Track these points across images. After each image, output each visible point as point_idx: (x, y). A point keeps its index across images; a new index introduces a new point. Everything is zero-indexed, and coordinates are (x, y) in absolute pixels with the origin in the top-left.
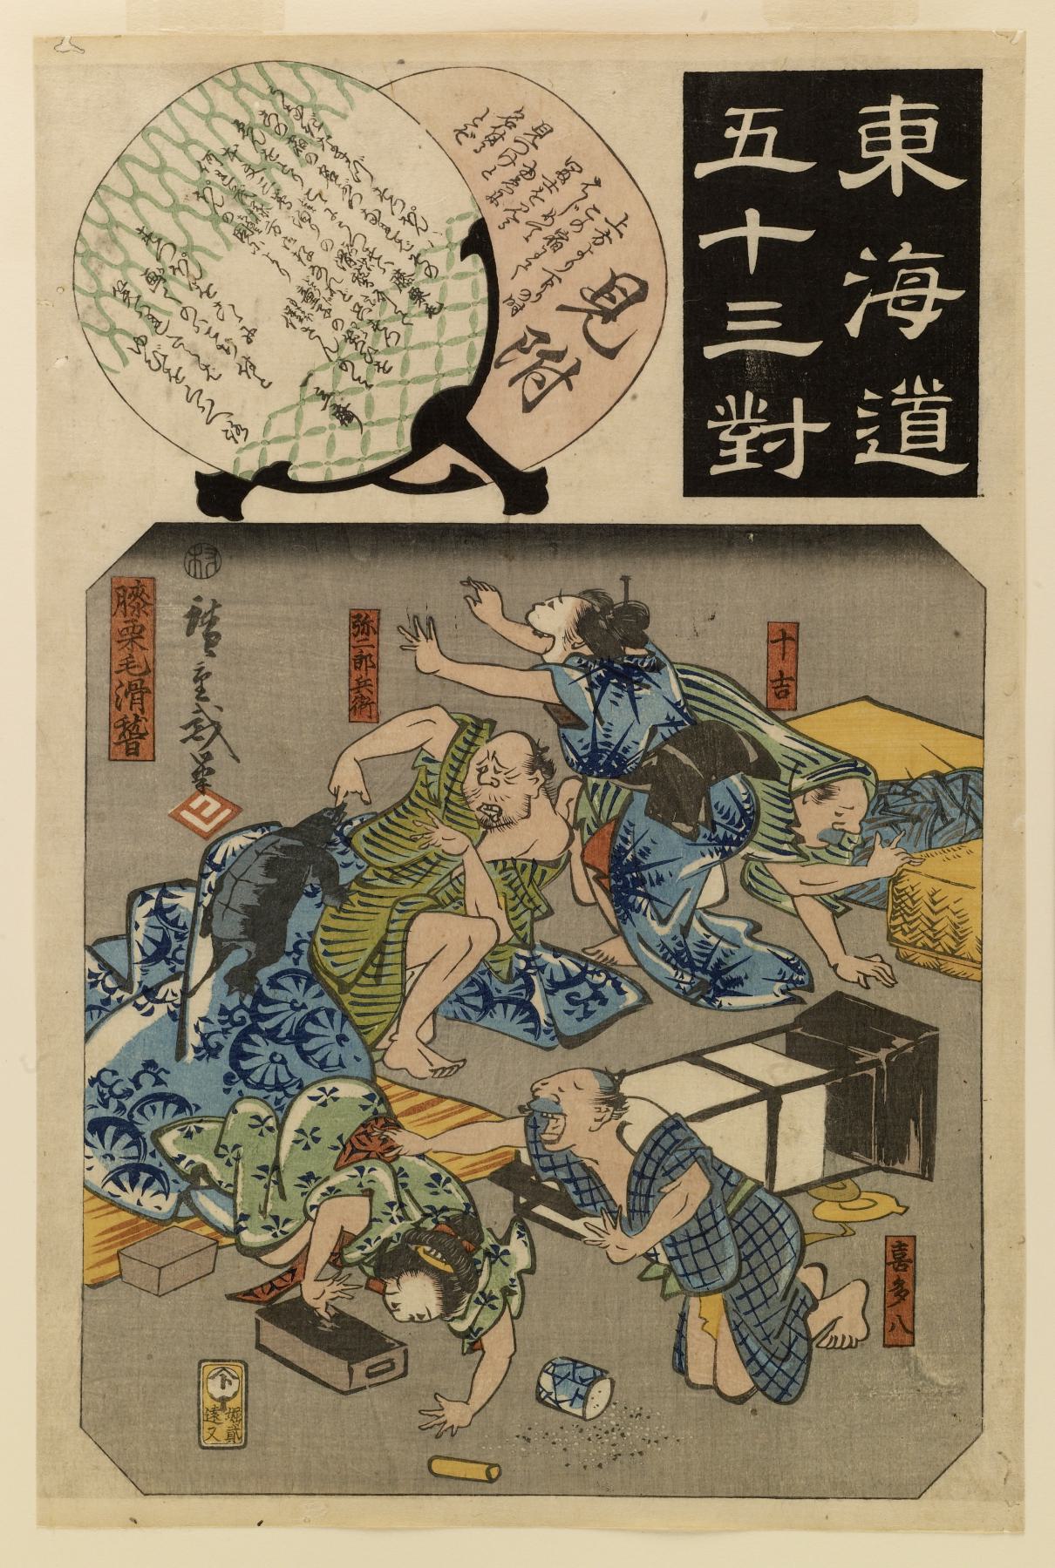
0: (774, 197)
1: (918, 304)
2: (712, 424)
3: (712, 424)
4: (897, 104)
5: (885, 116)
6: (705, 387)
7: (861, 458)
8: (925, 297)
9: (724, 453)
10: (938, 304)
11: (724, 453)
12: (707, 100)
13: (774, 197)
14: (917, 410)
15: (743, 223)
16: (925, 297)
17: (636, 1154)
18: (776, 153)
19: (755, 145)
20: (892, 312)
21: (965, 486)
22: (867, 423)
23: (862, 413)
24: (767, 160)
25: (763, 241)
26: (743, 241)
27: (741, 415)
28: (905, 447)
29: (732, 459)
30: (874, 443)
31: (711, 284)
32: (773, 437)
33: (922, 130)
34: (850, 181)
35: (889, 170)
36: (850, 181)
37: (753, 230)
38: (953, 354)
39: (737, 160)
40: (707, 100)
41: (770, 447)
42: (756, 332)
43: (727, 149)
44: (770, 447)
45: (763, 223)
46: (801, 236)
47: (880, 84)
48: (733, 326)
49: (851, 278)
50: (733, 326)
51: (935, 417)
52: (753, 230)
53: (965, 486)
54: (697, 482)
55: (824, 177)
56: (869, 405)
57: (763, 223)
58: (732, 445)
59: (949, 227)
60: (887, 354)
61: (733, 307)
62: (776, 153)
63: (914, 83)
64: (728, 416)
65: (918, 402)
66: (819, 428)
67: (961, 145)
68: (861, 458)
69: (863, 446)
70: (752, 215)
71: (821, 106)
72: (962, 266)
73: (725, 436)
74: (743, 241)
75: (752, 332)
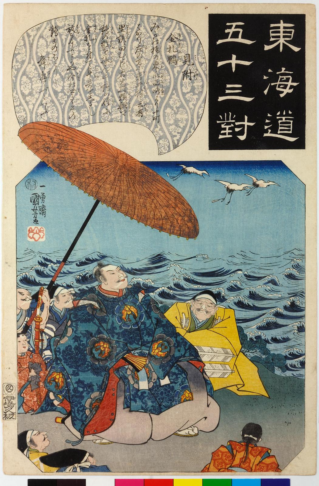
0: (241, 51)
1: (285, 87)
2: (218, 122)
3: (218, 122)
4: (282, 25)
5: (279, 28)
6: (217, 111)
7: (265, 135)
8: (287, 85)
9: (222, 132)
10: (291, 87)
11: (222, 132)
12: (218, 23)
13: (241, 51)
14: (284, 120)
15: (231, 59)
16: (287, 85)
17: (176, 328)
18: (242, 38)
19: (235, 35)
20: (278, 89)
21: (300, 144)
22: (267, 124)
23: (267, 121)
24: (240, 40)
25: (236, 65)
26: (230, 64)
27: (228, 119)
28: (279, 132)
29: (225, 134)
30: (270, 131)
31: (218, 79)
32: (239, 126)
33: (291, 32)
34: (267, 48)
35: (279, 44)
36: (267, 48)
37: (234, 61)
38: (296, 104)
39: (229, 40)
40: (218, 23)
41: (237, 130)
42: (233, 93)
43: (226, 36)
44: (237, 130)
45: (237, 59)
46: (247, 63)
47: (277, 18)
48: (227, 91)
49: (265, 78)
50: (227, 91)
51: (290, 123)
52: (234, 61)
53: (300, 144)
54: (215, 143)
55: (258, 46)
56: (269, 118)
57: (237, 59)
58: (225, 129)
59: (296, 64)
60: (275, 103)
61: (228, 86)
62: (242, 38)
63: (287, 18)
64: (224, 120)
65: (284, 118)
66: (252, 124)
67: (299, 38)
68: (265, 135)
69: (266, 131)
70: (234, 57)
71: (258, 25)
72: (299, 75)
73: (223, 126)
74: (230, 64)
75: (30, 51)
